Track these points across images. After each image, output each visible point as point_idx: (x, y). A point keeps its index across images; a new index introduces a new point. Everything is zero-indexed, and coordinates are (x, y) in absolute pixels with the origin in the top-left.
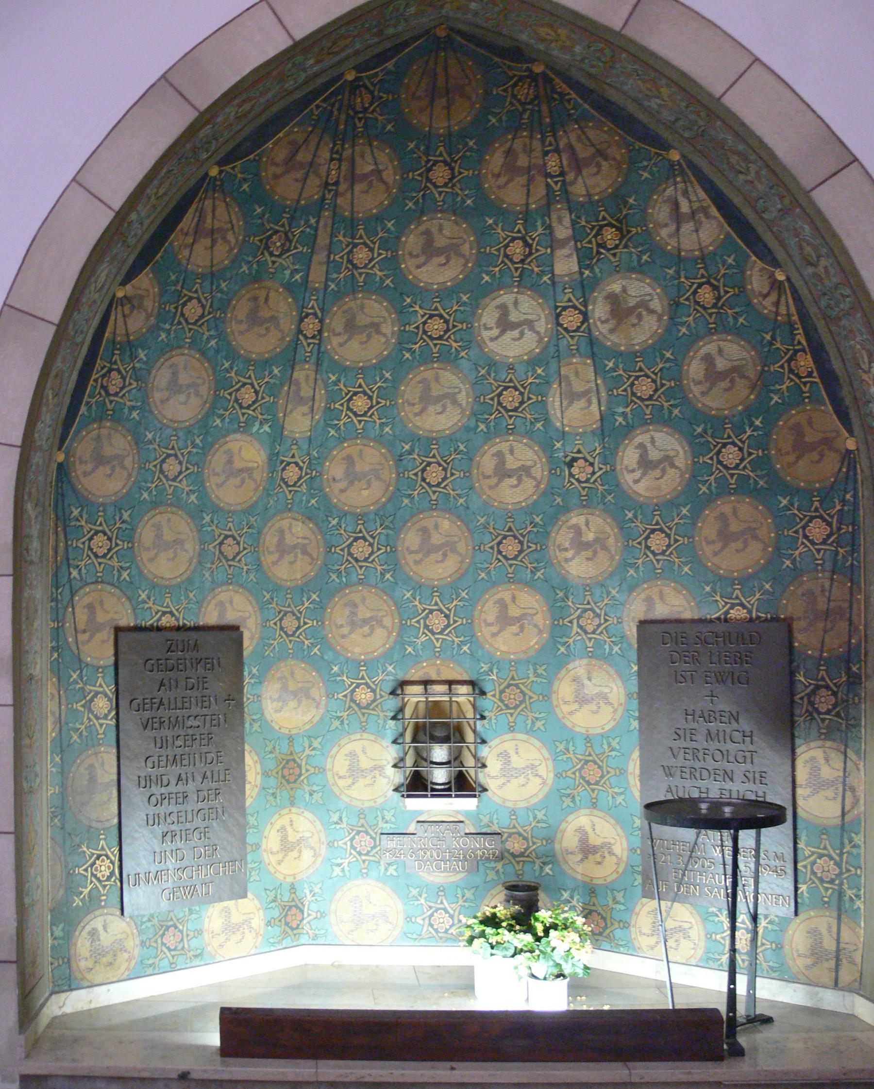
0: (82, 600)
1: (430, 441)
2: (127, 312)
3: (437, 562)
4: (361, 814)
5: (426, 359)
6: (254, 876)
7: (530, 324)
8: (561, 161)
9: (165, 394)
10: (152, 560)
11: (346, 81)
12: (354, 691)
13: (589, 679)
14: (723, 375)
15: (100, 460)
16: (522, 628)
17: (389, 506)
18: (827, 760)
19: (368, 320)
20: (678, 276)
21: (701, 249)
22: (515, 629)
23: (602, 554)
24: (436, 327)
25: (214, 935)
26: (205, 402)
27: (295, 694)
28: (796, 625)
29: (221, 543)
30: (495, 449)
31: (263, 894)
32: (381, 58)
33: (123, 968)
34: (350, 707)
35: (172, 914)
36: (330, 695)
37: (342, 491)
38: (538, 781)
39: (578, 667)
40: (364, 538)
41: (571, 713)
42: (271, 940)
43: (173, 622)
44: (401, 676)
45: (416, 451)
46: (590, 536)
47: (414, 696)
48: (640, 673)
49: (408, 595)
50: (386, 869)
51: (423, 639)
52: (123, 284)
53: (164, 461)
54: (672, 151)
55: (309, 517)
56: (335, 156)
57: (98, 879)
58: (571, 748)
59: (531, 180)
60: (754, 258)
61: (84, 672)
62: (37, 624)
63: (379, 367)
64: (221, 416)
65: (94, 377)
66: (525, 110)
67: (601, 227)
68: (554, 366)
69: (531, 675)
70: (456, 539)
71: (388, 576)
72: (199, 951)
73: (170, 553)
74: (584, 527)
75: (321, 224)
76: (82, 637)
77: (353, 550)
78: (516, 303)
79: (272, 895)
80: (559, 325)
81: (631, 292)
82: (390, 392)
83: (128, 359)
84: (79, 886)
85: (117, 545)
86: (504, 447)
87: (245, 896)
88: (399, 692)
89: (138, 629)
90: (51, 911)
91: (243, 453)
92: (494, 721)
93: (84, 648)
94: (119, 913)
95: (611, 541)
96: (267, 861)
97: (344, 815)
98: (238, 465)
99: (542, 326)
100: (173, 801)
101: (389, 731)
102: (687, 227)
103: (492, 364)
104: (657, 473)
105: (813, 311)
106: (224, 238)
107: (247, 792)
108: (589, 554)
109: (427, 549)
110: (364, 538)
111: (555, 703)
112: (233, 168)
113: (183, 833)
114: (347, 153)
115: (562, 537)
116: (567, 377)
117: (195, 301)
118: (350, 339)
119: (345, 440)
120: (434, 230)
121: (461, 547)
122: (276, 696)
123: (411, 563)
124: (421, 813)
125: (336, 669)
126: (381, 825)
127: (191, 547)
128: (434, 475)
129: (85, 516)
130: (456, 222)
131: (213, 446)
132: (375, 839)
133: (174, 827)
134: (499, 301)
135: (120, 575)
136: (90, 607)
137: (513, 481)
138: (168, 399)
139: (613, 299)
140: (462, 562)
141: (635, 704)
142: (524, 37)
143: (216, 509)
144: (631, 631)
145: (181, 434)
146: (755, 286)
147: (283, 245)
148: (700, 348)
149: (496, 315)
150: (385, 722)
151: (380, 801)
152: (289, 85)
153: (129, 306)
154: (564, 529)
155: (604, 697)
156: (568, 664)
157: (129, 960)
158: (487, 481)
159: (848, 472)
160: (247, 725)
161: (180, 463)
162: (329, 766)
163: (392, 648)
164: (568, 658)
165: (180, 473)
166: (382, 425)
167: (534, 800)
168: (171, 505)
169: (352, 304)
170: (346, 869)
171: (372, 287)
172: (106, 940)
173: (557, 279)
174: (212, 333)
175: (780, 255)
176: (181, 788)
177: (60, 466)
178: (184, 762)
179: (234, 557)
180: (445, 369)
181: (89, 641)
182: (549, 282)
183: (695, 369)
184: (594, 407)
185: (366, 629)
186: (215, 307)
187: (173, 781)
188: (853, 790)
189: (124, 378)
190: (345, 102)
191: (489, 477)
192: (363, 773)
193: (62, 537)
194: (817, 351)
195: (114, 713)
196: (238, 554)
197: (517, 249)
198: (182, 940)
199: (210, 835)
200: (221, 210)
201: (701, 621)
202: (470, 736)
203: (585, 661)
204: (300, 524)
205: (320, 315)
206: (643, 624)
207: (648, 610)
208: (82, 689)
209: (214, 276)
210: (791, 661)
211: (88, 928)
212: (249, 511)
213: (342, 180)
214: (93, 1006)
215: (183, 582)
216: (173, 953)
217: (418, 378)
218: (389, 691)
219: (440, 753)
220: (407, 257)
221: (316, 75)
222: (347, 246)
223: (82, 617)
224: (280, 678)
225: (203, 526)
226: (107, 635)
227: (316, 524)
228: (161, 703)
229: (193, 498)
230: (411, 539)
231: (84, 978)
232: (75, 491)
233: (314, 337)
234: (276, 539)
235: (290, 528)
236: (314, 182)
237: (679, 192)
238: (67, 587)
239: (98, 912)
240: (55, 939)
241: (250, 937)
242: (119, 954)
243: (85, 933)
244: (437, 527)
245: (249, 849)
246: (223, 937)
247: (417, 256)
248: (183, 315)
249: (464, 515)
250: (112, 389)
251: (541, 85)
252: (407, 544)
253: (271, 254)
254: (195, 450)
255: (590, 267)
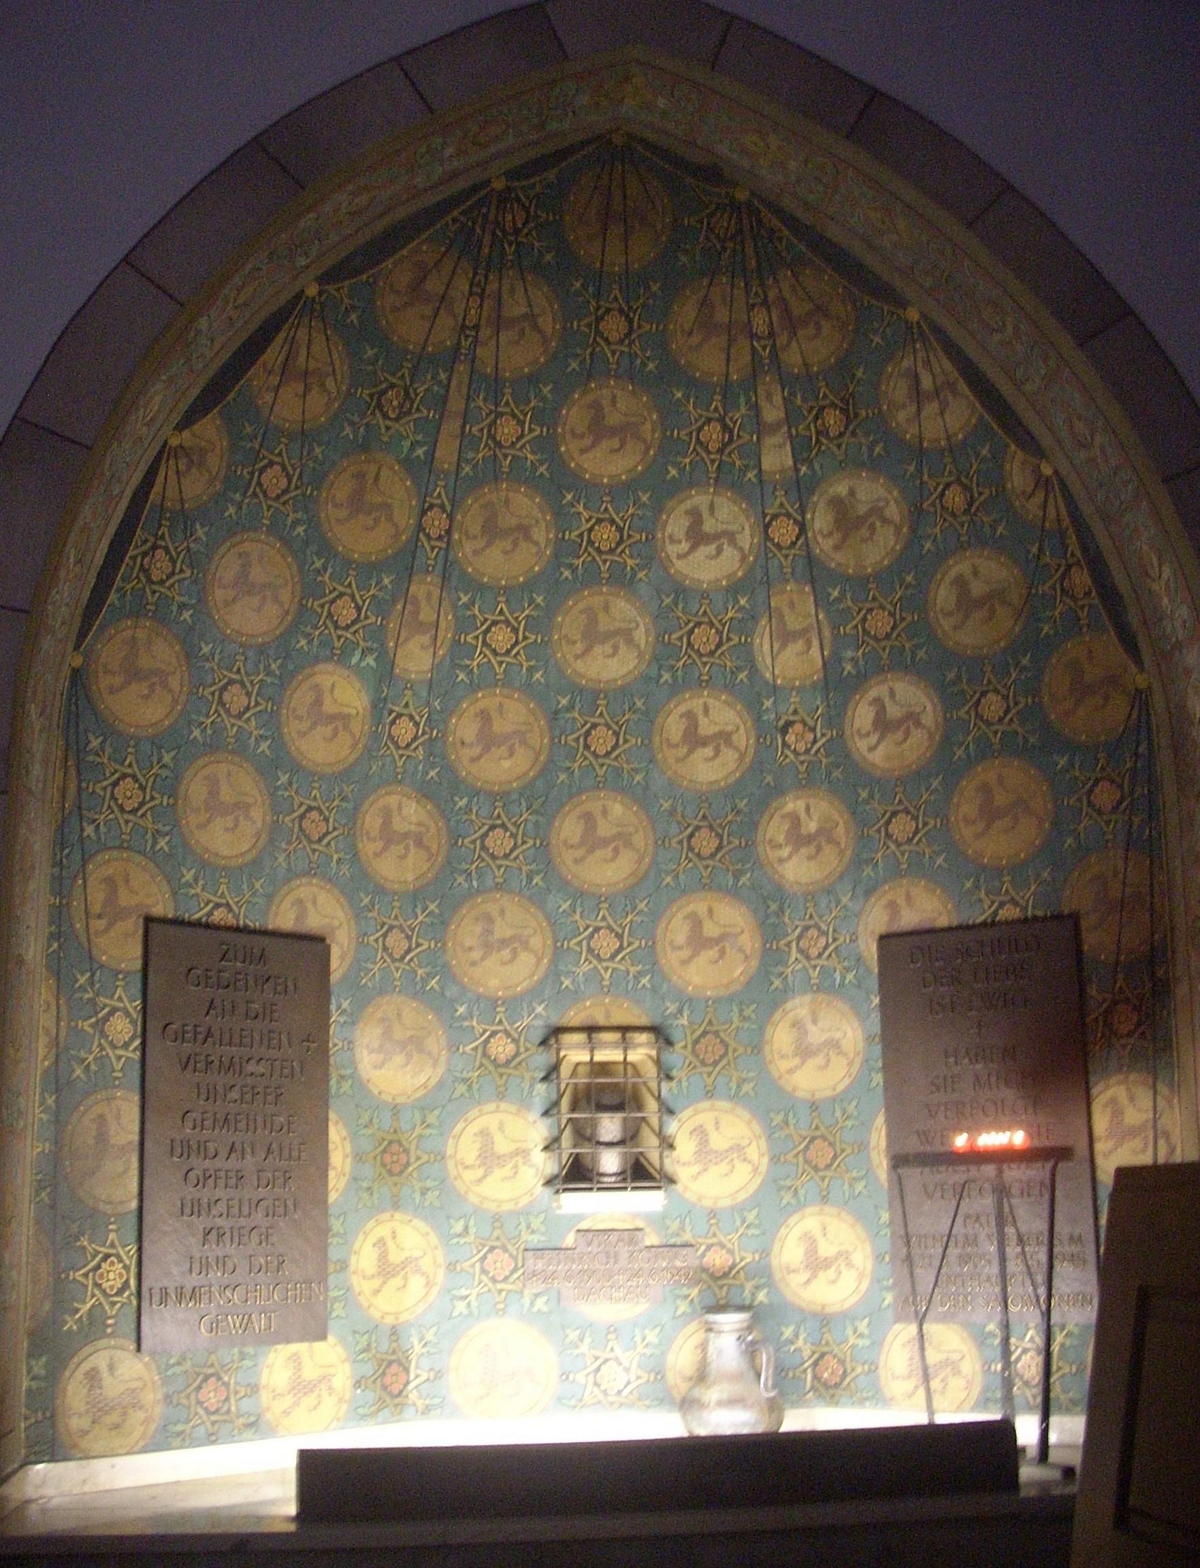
0: (101, 869)
1: (596, 694)
2: (182, 467)
3: (605, 861)
4: (497, 1219)
5: (591, 578)
6: (338, 1310)
7: (731, 537)
8: (770, 317)
9: (230, 593)
10: (201, 827)
11: (493, 190)
12: (487, 1041)
13: (815, 1022)
14: (980, 603)
15: (133, 673)
16: (722, 953)
17: (540, 783)
18: (1132, 1099)
19: (514, 522)
20: (919, 470)
21: (948, 439)
22: (712, 953)
23: (828, 849)
24: (606, 535)
25: (276, 1395)
26: (287, 612)
27: (403, 1045)
28: (1084, 923)
29: (302, 817)
30: (683, 708)
31: (350, 1338)
32: (539, 165)
33: (137, 1434)
34: (481, 1065)
35: (213, 1357)
36: (453, 1047)
37: (474, 760)
38: (747, 1168)
39: (799, 1006)
40: (503, 826)
41: (791, 1071)
42: (361, 1411)
43: (230, 920)
44: (556, 1020)
45: (578, 706)
46: (813, 826)
47: (575, 1053)
48: (883, 1004)
49: (565, 906)
50: (532, 1304)
51: (586, 967)
52: (181, 427)
53: (224, 688)
54: (910, 309)
55: (426, 792)
56: (475, 289)
57: (104, 1292)
58: (792, 1122)
59: (731, 341)
60: (1013, 447)
61: (97, 978)
62: (32, 886)
63: (530, 586)
64: (309, 637)
65: (131, 553)
66: (724, 249)
67: (822, 408)
68: (761, 596)
69: (735, 1019)
70: (631, 829)
71: (537, 879)
72: (253, 1419)
73: (229, 821)
74: (803, 815)
75: (454, 383)
76: (101, 924)
77: (489, 842)
78: (712, 508)
79: (363, 1341)
80: (767, 538)
81: (862, 495)
82: (542, 623)
83: (180, 535)
84: (74, 1299)
85: (152, 798)
86: (696, 704)
87: (322, 1336)
88: (552, 1041)
89: (177, 922)
90: (29, 1335)
91: (336, 691)
92: (685, 1084)
93: (101, 941)
94: (133, 1347)
95: (840, 830)
96: (357, 1290)
97: (472, 1222)
98: (329, 707)
99: (747, 539)
100: (221, 1182)
101: (537, 1100)
102: (931, 409)
103: (681, 591)
104: (899, 735)
105: (1087, 510)
106: (323, 385)
107: (331, 1184)
108: (812, 849)
109: (591, 842)
110: (503, 826)
111: (768, 1058)
112: (338, 290)
113: (236, 1234)
114: (492, 287)
115: (774, 829)
116: (779, 610)
117: (277, 468)
118: (489, 544)
119: (479, 688)
120: (606, 402)
121: (639, 840)
122: (376, 1045)
123: (570, 863)
124: (582, 1217)
125: (461, 1010)
126: (526, 1236)
127: (259, 815)
128: (602, 740)
129: (108, 750)
130: (633, 393)
131: (293, 677)
132: (515, 1258)
133: (219, 1222)
134: (688, 504)
135: (155, 842)
136: (110, 882)
137: (708, 751)
138: (234, 600)
139: (840, 507)
140: (640, 861)
141: (877, 1049)
142: (723, 149)
143: (296, 768)
144: (870, 950)
145: (250, 654)
146: (1016, 484)
147: (401, 406)
148: (950, 567)
149: (685, 523)
150: (532, 1086)
151: (524, 1201)
152: (419, 181)
153: (185, 460)
154: (776, 818)
155: (834, 1045)
156: (785, 1002)
157: (146, 1421)
158: (674, 751)
159: (1139, 716)
160: (333, 1082)
161: (249, 694)
162: (450, 1151)
163: (541, 982)
164: (786, 992)
165: (248, 708)
166: (531, 670)
167: (742, 1196)
168: (232, 752)
169: (494, 497)
170: (474, 1304)
171: (522, 476)
172: (112, 1387)
173: (765, 477)
174: (299, 515)
175: (1046, 441)
176: (233, 1163)
177: (76, 672)
178: (242, 1125)
179: (320, 840)
180: (618, 596)
181: (107, 930)
182: (754, 480)
183: (944, 595)
184: (815, 651)
185: (506, 953)
186: (305, 480)
187: (223, 1153)
188: (1167, 1136)
189: (173, 561)
190: (491, 217)
191: (676, 746)
192: (500, 1160)
193: (73, 772)
194: (1096, 564)
195: (137, 1042)
196: (325, 835)
197: (713, 434)
198: (227, 1399)
199: (274, 1239)
200: (319, 346)
201: (960, 928)
202: (652, 1105)
203: (808, 998)
204: (414, 805)
205: (449, 508)
206: (884, 939)
207: (891, 920)
208: (92, 1001)
209: (304, 436)
210: (1080, 971)
211: (86, 1366)
212: (344, 776)
213: (483, 321)
214: (86, 1489)
215: (246, 865)
216: (213, 1418)
217: (581, 606)
218: (537, 1042)
219: (610, 1126)
220: (568, 436)
221: (453, 176)
222: (488, 415)
223: (97, 896)
224: (383, 1020)
225: (277, 788)
226: (133, 926)
227: (438, 806)
228: (209, 1034)
229: (264, 746)
230: (569, 828)
231: (75, 1446)
232: (95, 712)
233: (440, 538)
234: (380, 821)
235: (400, 808)
236: (445, 323)
237: (920, 364)
238: (77, 848)
239: (102, 1343)
240: (33, 1379)
241: (329, 1402)
242: (131, 1411)
243: (79, 1374)
244: (605, 812)
245: (331, 1268)
246: (288, 1400)
247: (582, 436)
248: (259, 484)
249: (642, 798)
250: (156, 575)
251: (745, 216)
252: (563, 835)
253: (385, 416)
254: (269, 680)
255: (809, 462)
